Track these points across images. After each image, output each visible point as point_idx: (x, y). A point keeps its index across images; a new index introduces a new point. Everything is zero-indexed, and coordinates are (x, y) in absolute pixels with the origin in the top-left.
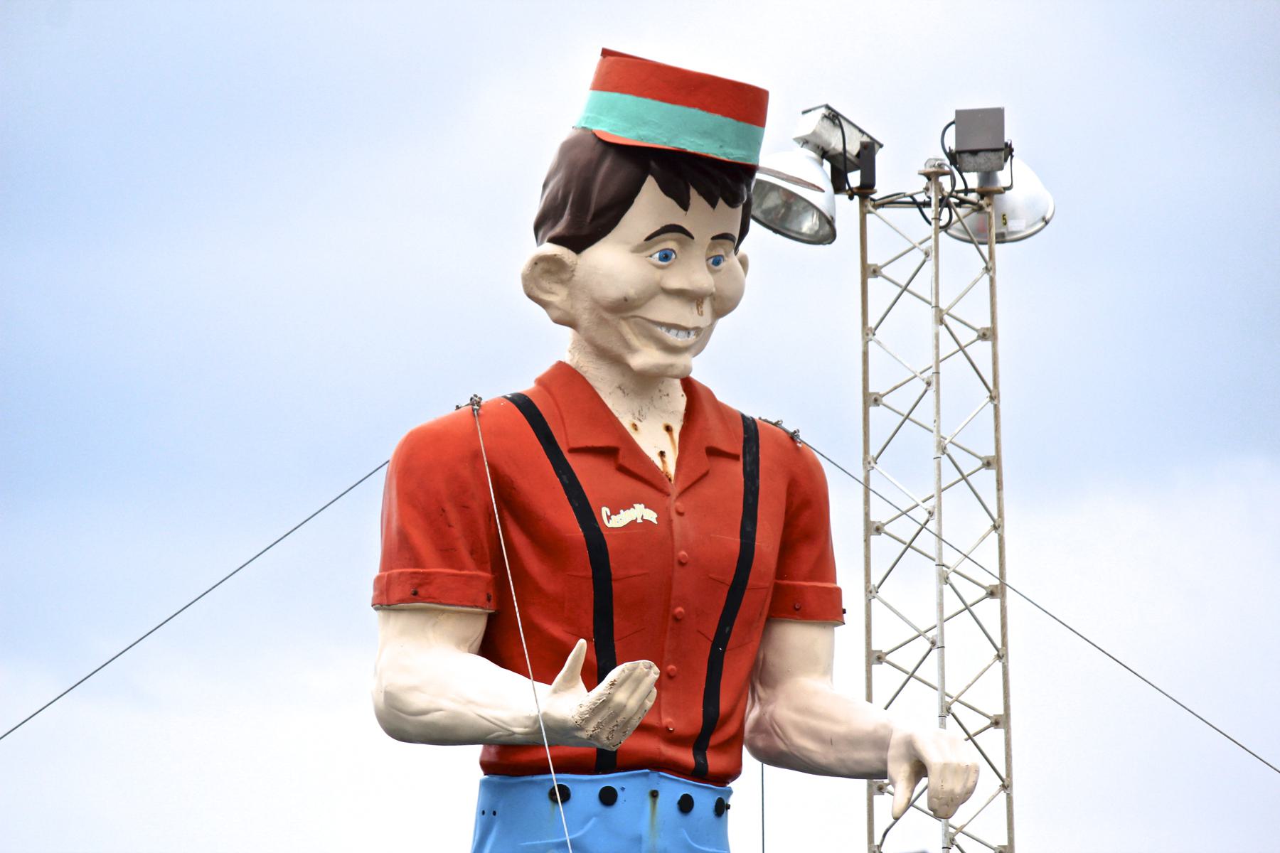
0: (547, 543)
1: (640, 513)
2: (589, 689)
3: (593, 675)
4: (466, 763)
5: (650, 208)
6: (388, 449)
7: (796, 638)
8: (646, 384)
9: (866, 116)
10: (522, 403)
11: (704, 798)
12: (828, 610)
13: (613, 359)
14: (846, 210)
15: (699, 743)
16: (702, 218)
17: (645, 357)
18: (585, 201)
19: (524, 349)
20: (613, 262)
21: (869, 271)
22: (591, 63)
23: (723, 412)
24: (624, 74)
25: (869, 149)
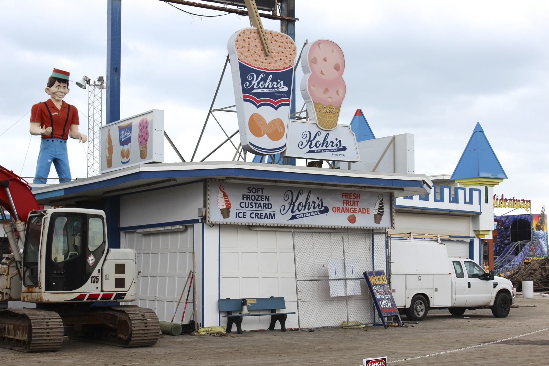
0: (46, 116)
1: (56, 113)
2: (131, 123)
3: (46, 128)
4: (40, 137)
5: (57, 83)
6: (76, 106)
7: (74, 126)
8: (58, 101)
9: (89, 77)
10: (45, 103)
11: (63, 141)
12: (78, 123)
13: (54, 98)
14: (87, 86)
15: (63, 136)
16: (62, 85)
17: (57, 98)
18: (52, 82)
19: (45, 97)
20: (54, 89)
21: (89, 92)
22: (53, 70)
23: (67, 104)
24: (56, 71)
25: (89, 80)
